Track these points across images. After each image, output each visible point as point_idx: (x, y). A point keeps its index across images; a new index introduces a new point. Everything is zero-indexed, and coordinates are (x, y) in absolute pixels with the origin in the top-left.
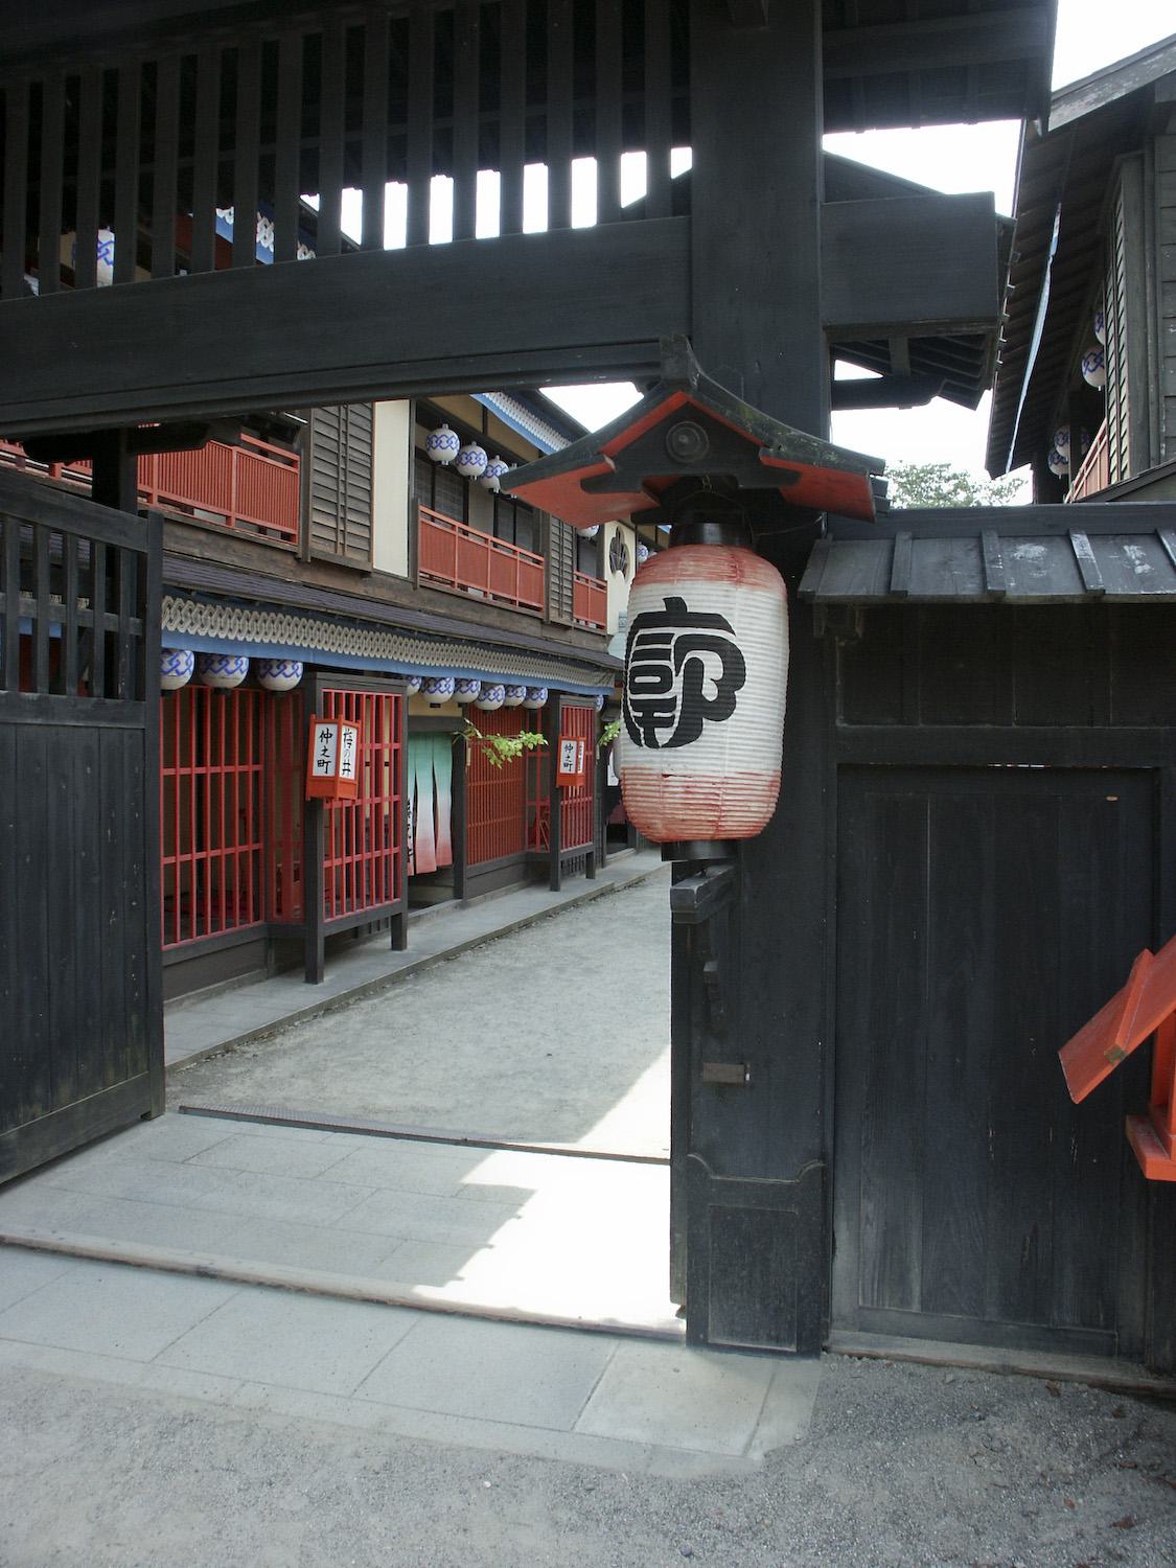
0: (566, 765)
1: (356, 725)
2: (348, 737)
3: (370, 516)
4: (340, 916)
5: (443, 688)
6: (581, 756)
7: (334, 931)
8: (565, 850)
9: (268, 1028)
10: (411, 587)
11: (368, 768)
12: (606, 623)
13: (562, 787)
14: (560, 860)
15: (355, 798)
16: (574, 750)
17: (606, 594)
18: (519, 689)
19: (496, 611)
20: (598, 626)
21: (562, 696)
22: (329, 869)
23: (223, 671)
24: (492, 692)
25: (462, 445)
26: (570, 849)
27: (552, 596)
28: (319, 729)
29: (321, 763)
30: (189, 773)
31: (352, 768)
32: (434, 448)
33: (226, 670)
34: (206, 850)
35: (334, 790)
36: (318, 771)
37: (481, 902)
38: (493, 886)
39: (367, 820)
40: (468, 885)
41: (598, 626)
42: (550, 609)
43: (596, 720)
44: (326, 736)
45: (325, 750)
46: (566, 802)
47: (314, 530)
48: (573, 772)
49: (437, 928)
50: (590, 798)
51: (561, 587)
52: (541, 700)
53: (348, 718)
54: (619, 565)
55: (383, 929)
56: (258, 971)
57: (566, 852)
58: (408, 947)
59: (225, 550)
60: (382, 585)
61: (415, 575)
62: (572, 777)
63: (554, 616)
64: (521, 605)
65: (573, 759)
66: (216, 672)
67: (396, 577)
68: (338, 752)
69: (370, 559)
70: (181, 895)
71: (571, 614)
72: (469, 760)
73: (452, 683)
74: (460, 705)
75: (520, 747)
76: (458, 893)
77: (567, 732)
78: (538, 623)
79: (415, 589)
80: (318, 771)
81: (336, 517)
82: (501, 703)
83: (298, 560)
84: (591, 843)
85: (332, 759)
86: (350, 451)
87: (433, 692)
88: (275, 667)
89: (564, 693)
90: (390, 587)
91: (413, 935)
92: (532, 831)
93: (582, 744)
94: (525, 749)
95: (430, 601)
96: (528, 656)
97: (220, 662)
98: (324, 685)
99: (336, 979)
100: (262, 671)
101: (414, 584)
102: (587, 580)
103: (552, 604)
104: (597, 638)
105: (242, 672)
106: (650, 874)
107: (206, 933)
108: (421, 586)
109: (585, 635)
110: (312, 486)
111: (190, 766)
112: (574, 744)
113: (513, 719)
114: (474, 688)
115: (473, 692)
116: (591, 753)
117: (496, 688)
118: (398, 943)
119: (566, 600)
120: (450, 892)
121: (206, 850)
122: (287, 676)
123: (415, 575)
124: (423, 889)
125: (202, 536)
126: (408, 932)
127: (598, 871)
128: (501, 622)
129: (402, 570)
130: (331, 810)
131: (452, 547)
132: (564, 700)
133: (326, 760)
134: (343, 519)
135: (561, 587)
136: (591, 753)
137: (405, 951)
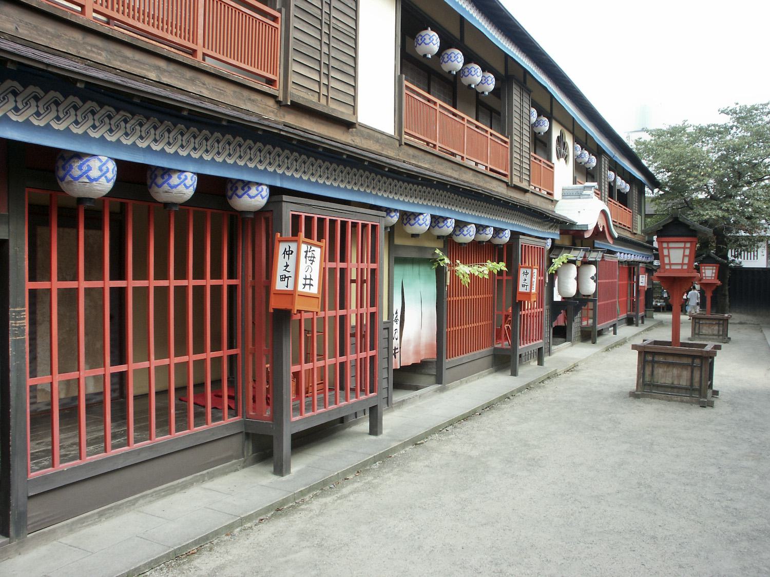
0: (523, 286)
1: (319, 243)
2: (309, 254)
3: (355, 78)
4: (310, 414)
5: (421, 222)
6: (535, 280)
7: (302, 428)
8: (523, 346)
9: (195, 543)
10: (397, 143)
11: (354, 285)
12: (553, 191)
13: (520, 302)
14: (518, 354)
15: (318, 310)
16: (530, 274)
17: (553, 172)
18: (488, 229)
19: (471, 172)
20: (548, 193)
21: (521, 236)
22: (297, 375)
23: (166, 185)
24: (465, 229)
25: (464, 64)
26: (526, 345)
27: (514, 167)
28: (282, 247)
29: (283, 278)
30: (76, 287)
31: (315, 282)
32: (420, 45)
33: (248, 195)
34: (188, 355)
35: (293, 303)
36: (280, 285)
37: (457, 386)
38: (466, 373)
39: (352, 327)
40: (446, 374)
41: (548, 193)
42: (514, 176)
43: (546, 254)
44: (288, 253)
45: (287, 266)
46: (523, 312)
47: (293, 78)
48: (528, 291)
49: (409, 413)
50: (541, 310)
51: (521, 162)
52: (506, 237)
53: (309, 235)
54: (562, 155)
55: (361, 416)
56: (234, 461)
57: (522, 348)
58: (384, 432)
59: (192, 81)
60: (369, 137)
61: (400, 134)
62: (528, 295)
63: (516, 181)
64: (491, 170)
65: (528, 281)
66: (159, 186)
67: (382, 133)
68: (301, 269)
69: (355, 113)
70: (212, 382)
71: (529, 181)
72: (448, 281)
73: (429, 218)
74: (439, 237)
75: (486, 272)
76: (439, 380)
77: (525, 262)
78: (504, 185)
79: (400, 145)
80: (280, 285)
81: (319, 72)
82: (473, 238)
83: (278, 103)
84: (541, 341)
85: (292, 274)
86: (333, 21)
87: (413, 225)
88: (240, 188)
89: (524, 234)
90: (377, 141)
91: (389, 420)
92: (499, 332)
93: (535, 271)
94: (491, 273)
95: (414, 157)
96: (418, 184)
97: (443, 222)
98: (289, 209)
99: (305, 467)
100: (230, 193)
101: (400, 141)
102: (540, 161)
103: (514, 172)
104: (547, 201)
105: (427, 226)
106: (581, 361)
107: (189, 429)
108: (405, 144)
109: (539, 198)
110: (291, 40)
111: (103, 279)
112: (529, 271)
113: (480, 250)
114: (449, 224)
115: (187, 187)
116: (542, 278)
117: (469, 226)
118: (375, 429)
119: (525, 171)
120: (433, 379)
121: (188, 355)
122: (251, 197)
123: (400, 134)
124: (407, 377)
125: (162, 64)
126: (384, 418)
127: (546, 359)
128: (475, 181)
129: (388, 126)
130: (300, 320)
131: (433, 119)
132: (523, 240)
133: (288, 275)
134: (327, 76)
135: (521, 162)
136: (542, 278)
137: (380, 437)
